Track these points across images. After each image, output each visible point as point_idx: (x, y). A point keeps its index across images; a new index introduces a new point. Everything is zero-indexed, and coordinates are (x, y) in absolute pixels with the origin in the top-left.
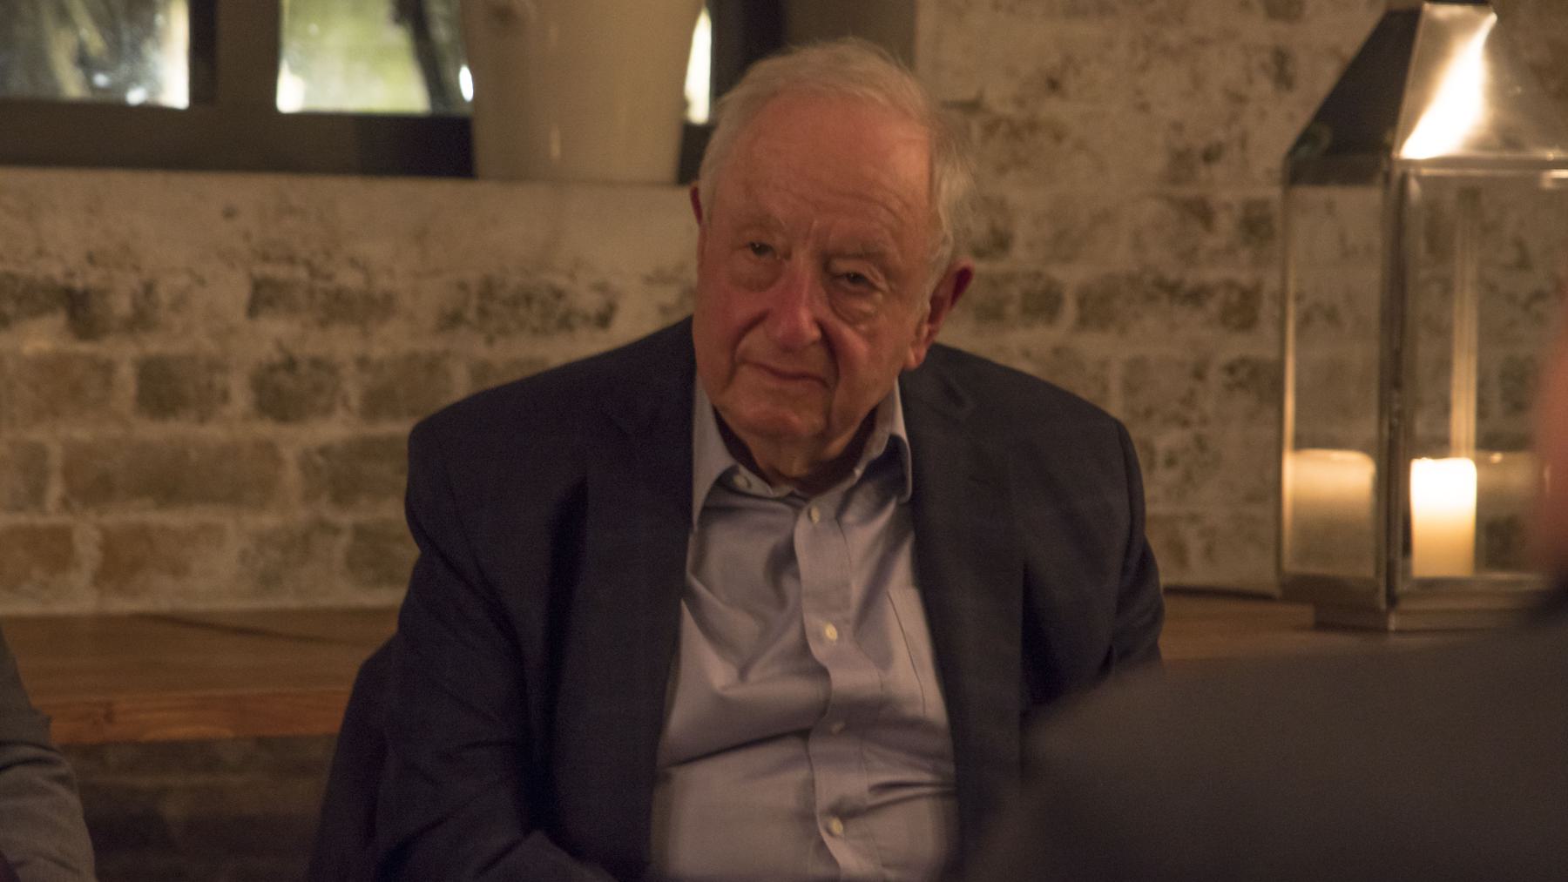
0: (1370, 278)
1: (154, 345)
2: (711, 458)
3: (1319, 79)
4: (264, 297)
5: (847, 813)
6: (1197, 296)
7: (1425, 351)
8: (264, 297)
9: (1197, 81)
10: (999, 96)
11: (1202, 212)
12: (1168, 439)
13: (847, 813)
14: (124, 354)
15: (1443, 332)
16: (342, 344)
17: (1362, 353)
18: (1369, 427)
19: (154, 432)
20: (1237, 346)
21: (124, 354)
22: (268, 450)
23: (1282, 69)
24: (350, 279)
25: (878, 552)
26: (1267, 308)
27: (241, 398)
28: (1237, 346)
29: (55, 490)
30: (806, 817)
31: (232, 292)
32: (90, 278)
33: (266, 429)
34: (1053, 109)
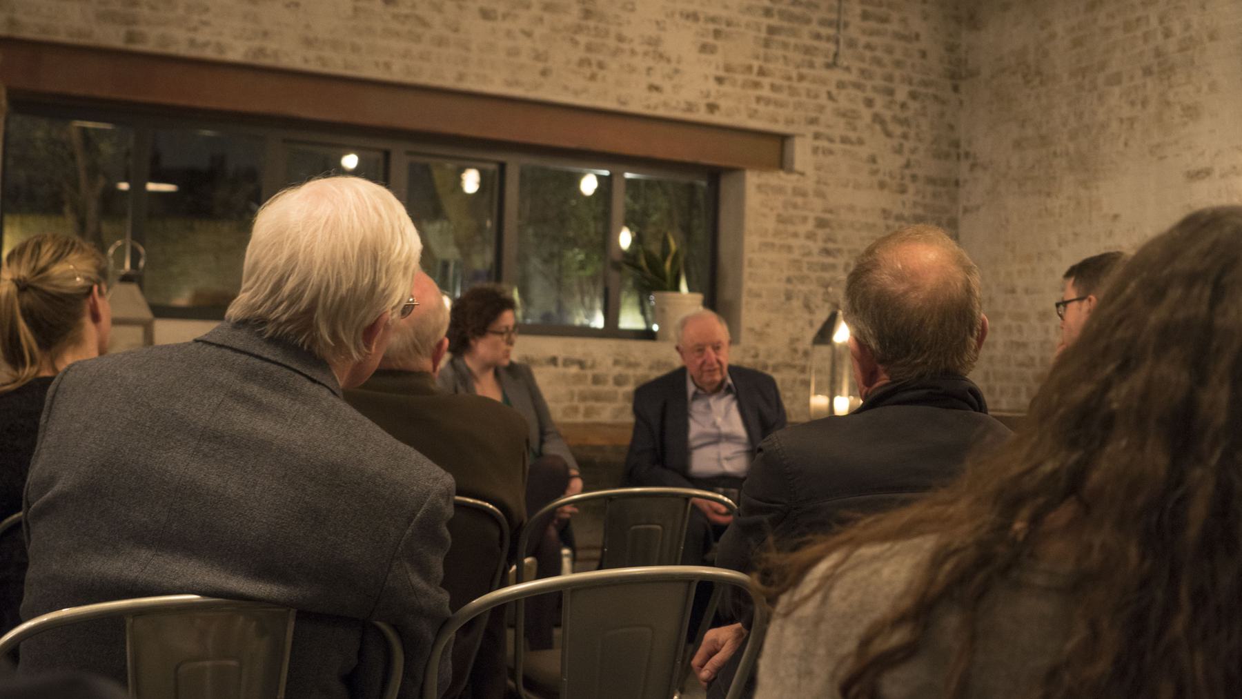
0: (827, 365)
1: (596, 371)
2: (691, 388)
3: (818, 326)
4: (616, 363)
5: (727, 459)
6: (794, 367)
7: (838, 378)
8: (616, 363)
9: (942, 115)
10: (757, 327)
11: (795, 351)
12: (789, 394)
13: (727, 459)
14: (589, 373)
15: (841, 375)
16: (630, 372)
17: (826, 378)
18: (828, 392)
19: (595, 388)
20: (802, 377)
21: (589, 373)
22: (616, 393)
23: (811, 324)
24: (632, 360)
25: (377, 279)
26: (808, 370)
27: (611, 381)
28: (802, 377)
29: (576, 398)
30: (719, 460)
31: (610, 362)
32: (583, 358)
33: (616, 388)
34: (770, 330)
